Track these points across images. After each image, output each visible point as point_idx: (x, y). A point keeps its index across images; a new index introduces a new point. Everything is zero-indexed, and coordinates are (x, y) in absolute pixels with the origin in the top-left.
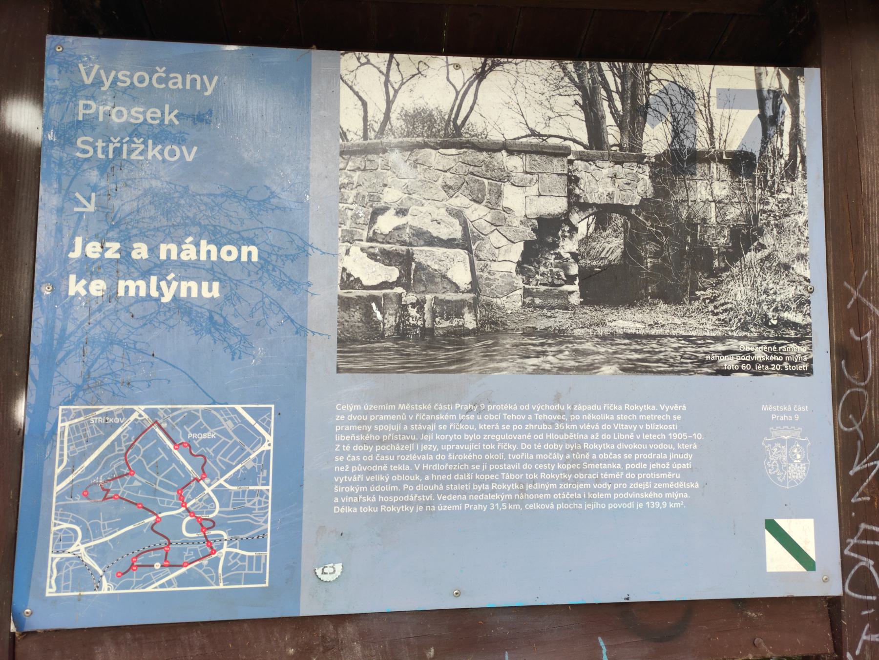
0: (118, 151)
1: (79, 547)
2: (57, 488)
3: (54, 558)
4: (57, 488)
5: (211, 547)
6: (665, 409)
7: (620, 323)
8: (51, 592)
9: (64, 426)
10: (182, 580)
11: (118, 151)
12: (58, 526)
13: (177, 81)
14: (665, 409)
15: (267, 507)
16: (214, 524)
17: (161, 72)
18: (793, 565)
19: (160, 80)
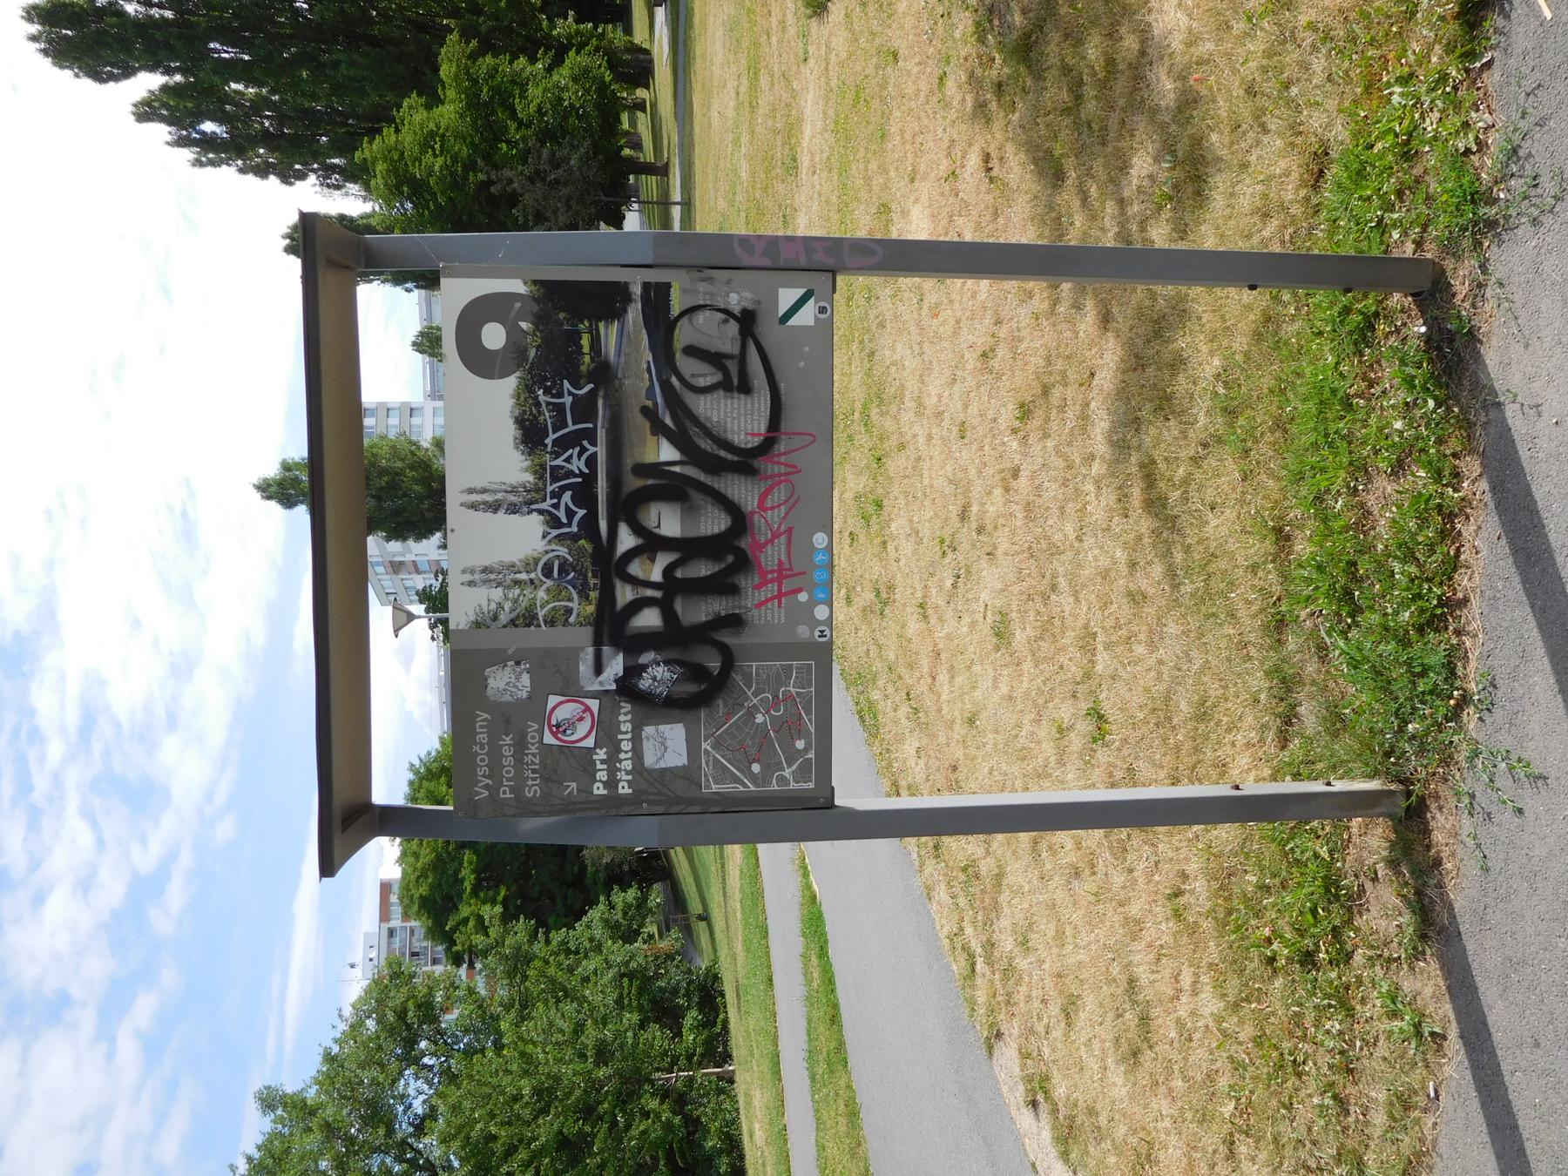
0: (534, 771)
1: (787, 773)
2: (752, 788)
3: (793, 785)
4: (752, 788)
5: (789, 697)
6: (487, 787)
7: (759, 1135)
8: (811, 785)
9: (715, 788)
10: (808, 713)
11: (534, 771)
12: (775, 786)
13: (482, 737)
14: (487, 787)
15: (591, 436)
16: (776, 697)
17: (476, 748)
18: (783, 309)
19: (482, 748)
